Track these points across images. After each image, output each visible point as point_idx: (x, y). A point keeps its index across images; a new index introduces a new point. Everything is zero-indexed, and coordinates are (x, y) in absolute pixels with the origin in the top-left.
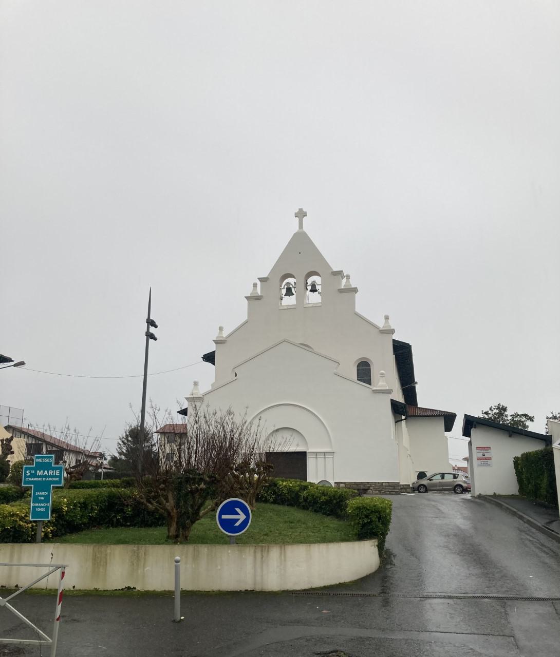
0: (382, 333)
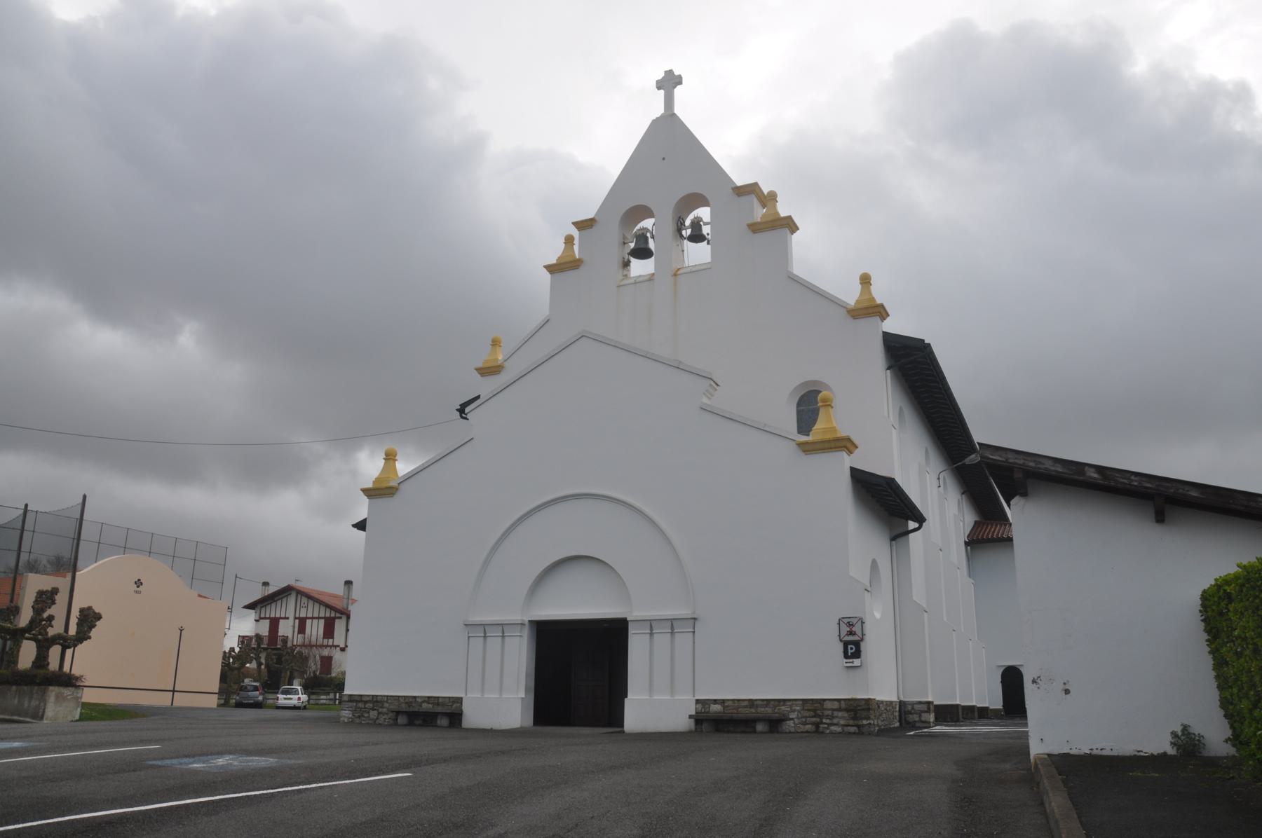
0: (855, 317)
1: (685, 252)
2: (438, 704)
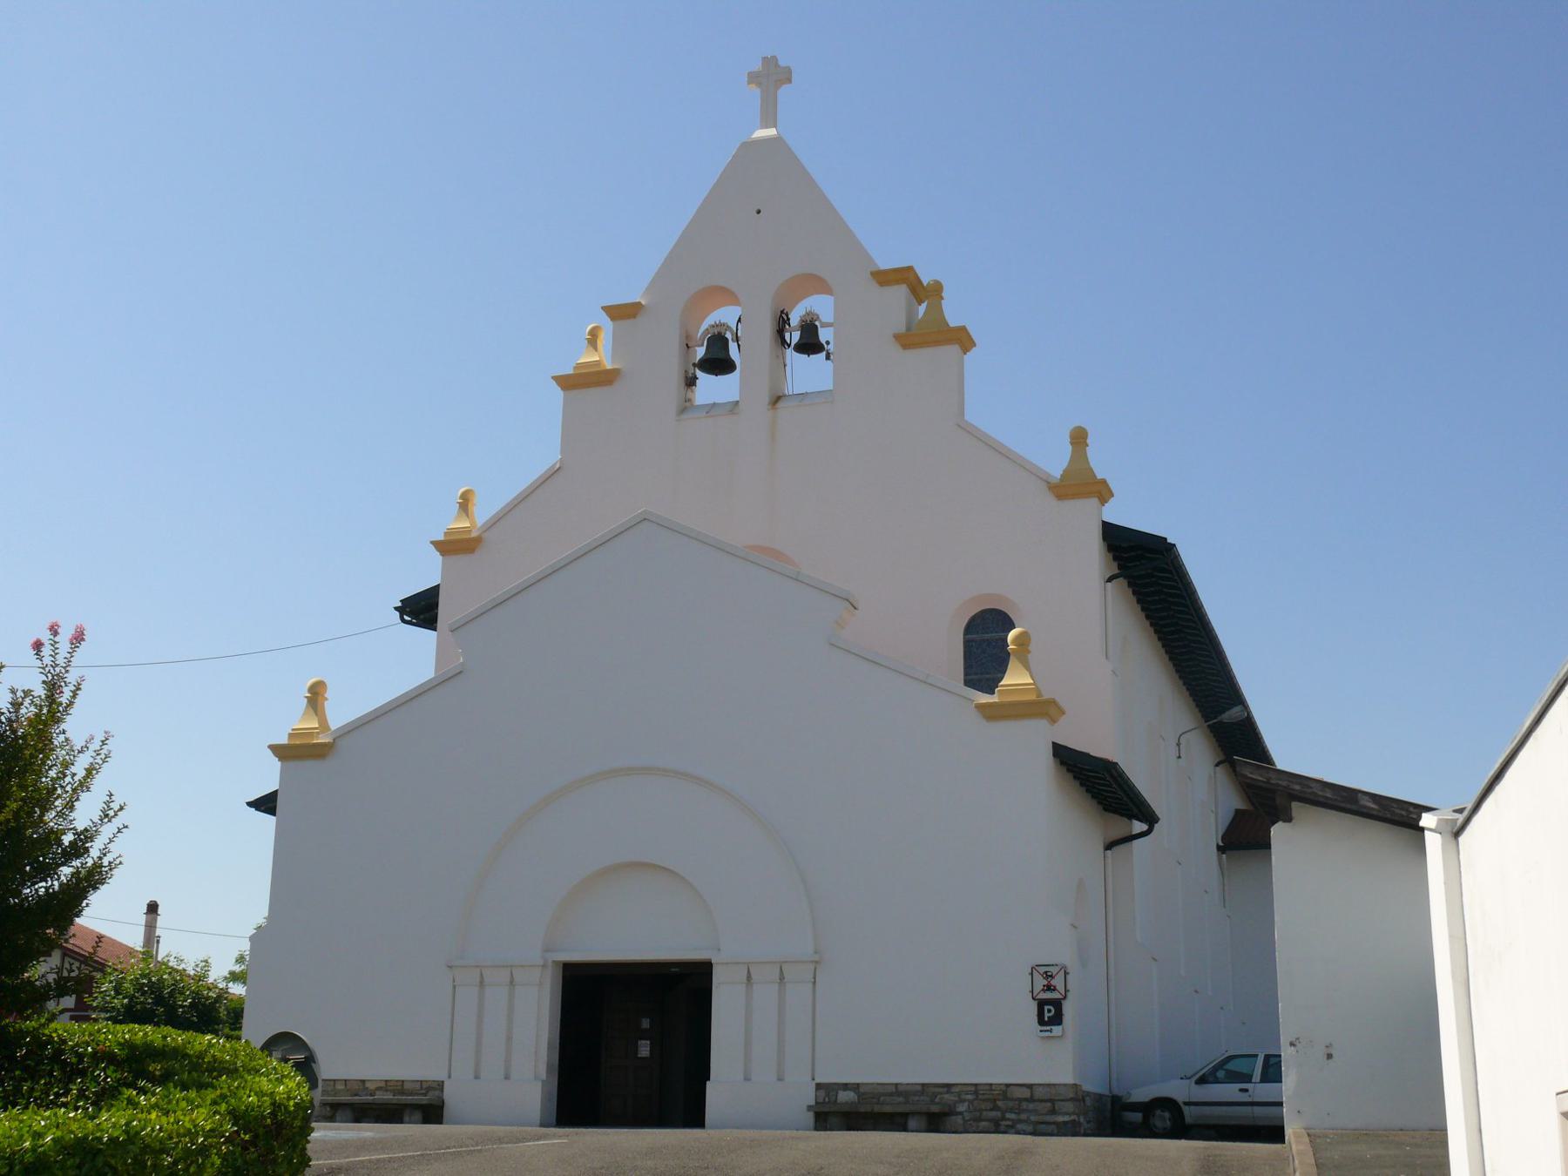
1: (788, 368)
2: (402, 1092)
